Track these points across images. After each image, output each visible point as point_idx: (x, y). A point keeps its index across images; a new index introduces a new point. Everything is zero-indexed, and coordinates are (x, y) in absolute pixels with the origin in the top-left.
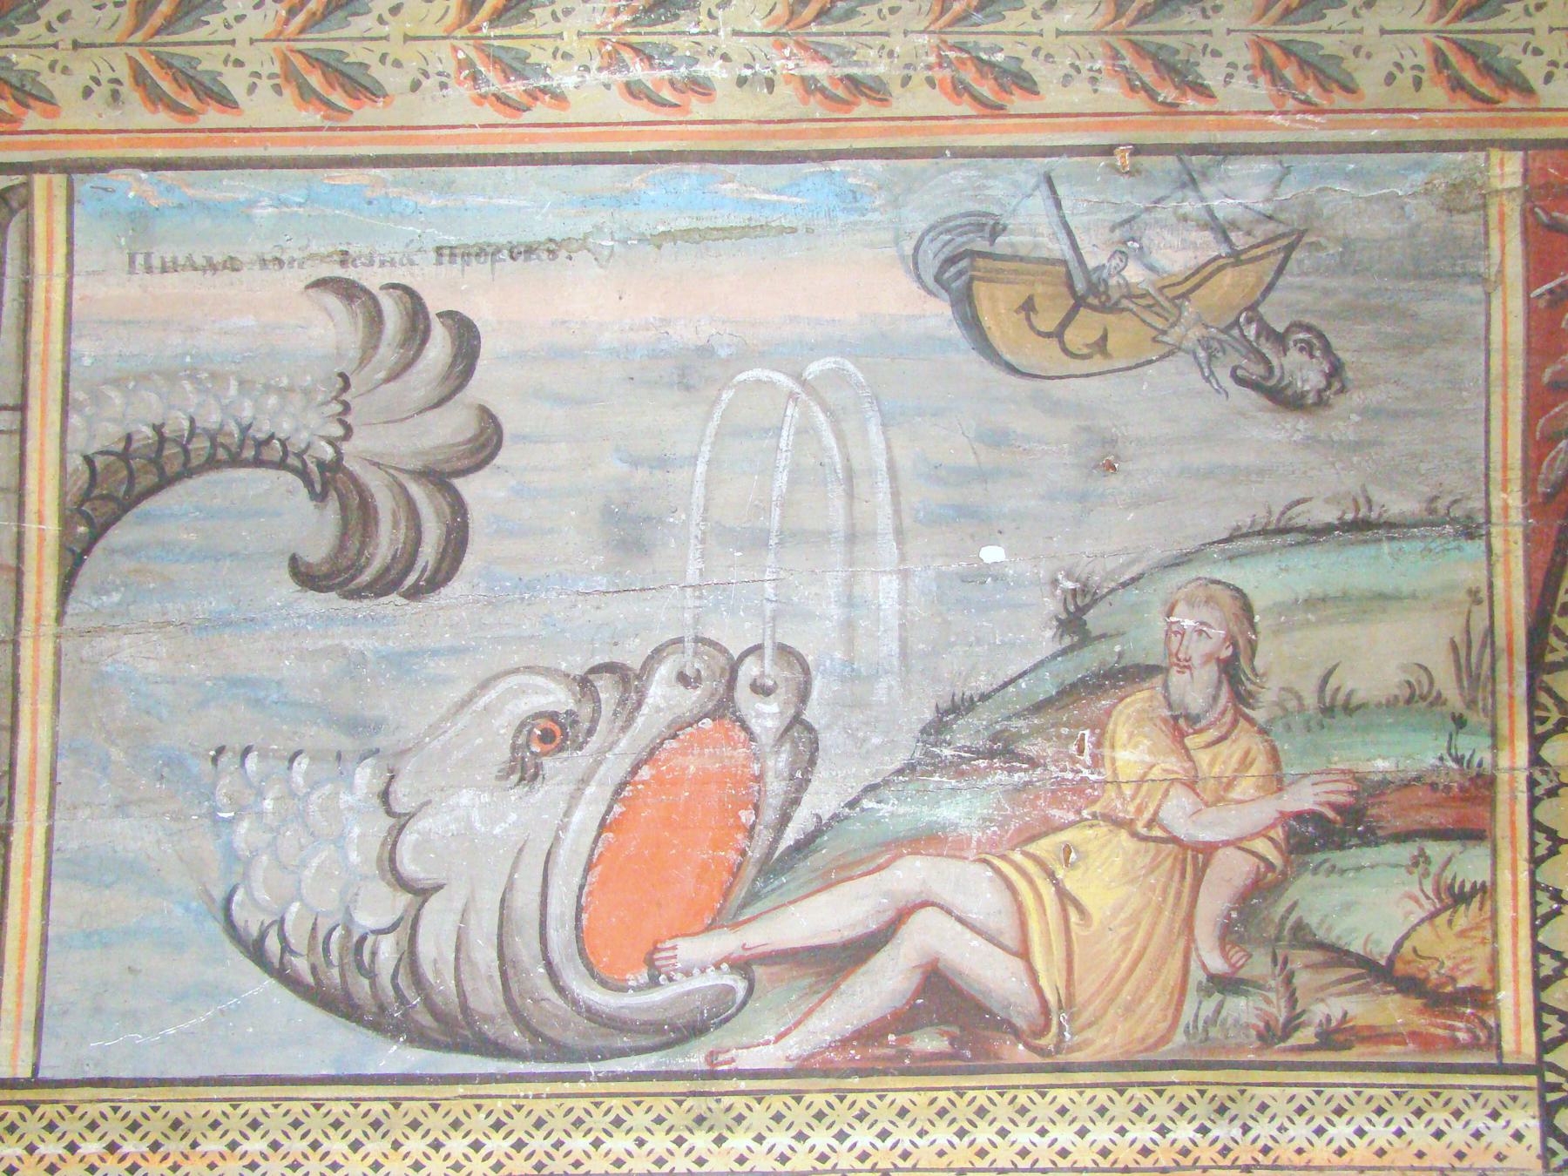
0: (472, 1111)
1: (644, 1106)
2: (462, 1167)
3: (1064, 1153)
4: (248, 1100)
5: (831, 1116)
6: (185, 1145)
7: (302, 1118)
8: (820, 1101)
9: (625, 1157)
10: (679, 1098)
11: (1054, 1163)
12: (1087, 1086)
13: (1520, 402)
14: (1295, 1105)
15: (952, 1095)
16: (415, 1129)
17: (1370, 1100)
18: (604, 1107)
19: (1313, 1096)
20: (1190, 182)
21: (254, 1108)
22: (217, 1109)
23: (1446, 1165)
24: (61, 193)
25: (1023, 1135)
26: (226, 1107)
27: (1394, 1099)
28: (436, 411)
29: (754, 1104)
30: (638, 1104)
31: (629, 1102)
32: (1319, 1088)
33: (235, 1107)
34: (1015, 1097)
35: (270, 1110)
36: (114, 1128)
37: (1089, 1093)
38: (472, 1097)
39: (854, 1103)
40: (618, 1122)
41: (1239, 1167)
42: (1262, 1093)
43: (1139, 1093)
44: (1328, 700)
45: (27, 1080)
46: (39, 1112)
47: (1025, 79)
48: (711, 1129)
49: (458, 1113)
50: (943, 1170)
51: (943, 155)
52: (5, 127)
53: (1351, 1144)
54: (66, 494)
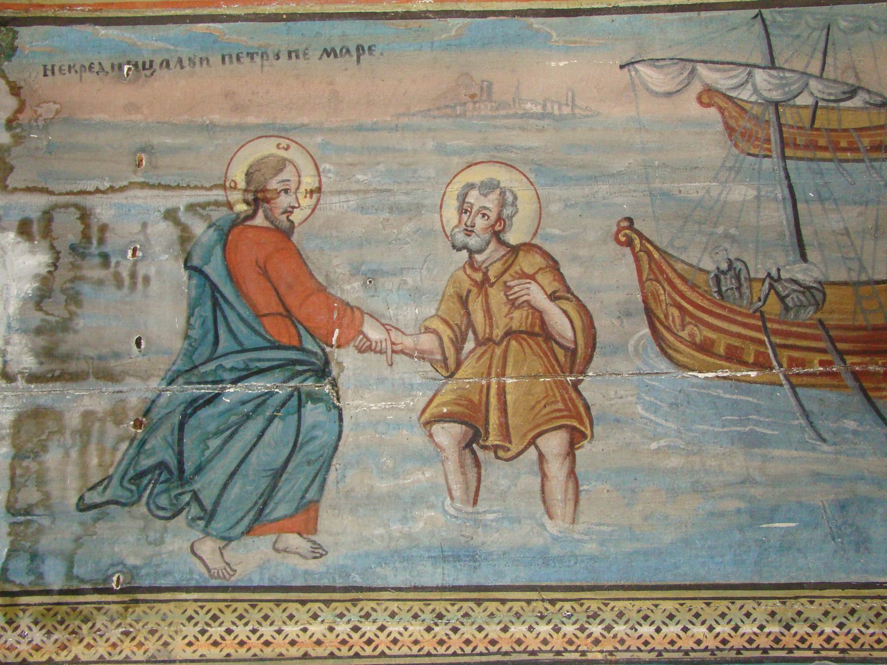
1: (231, 609)
2: (806, 640)
3: (493, 642)
5: (323, 616)
6: (718, 629)
9: (676, 639)
10: (708, 602)
11: (487, 649)
12: (738, 599)
14: (874, 612)
17: (235, 610)
18: (206, 609)
19: (423, 607)
20: (375, 123)
21: (440, 607)
23: (612, 649)
25: (699, 631)
29: (449, 607)
30: (228, 607)
31: (222, 605)
34: (461, 607)
35: (449, 607)
36: (382, 617)
37: (460, 604)
38: (653, 599)
40: (748, 615)
41: (527, 652)
42: (619, 605)
47: (747, 135)
49: (215, 611)
50: (221, 661)
52: (886, 138)
53: (653, 638)
54: (204, 208)
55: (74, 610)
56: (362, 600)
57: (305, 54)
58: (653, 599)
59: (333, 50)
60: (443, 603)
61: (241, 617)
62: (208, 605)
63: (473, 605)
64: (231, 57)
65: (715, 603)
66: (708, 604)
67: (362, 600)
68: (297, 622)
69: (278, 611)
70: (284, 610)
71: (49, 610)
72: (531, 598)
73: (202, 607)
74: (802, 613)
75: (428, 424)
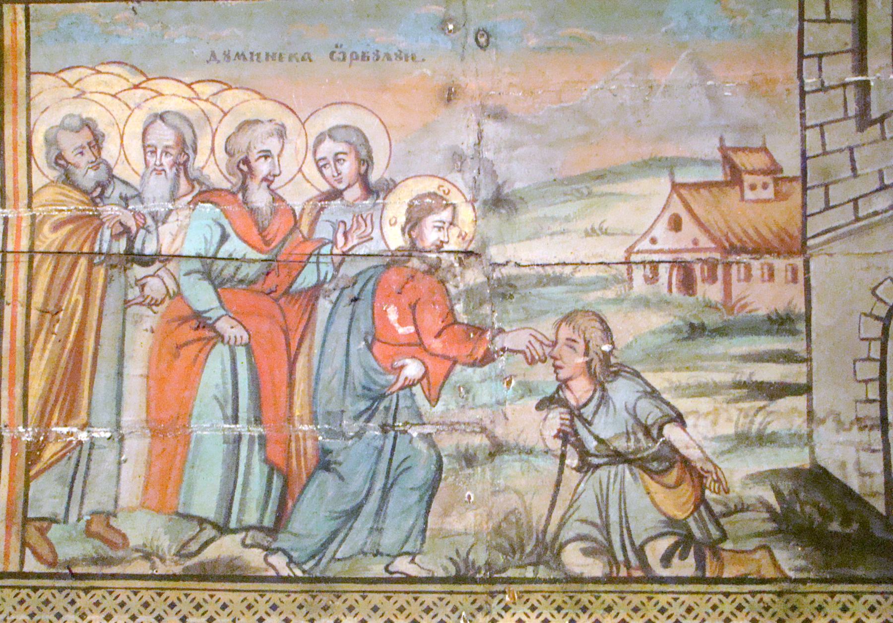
0: (412, 601)
1: (626, 601)
4: (395, 592)
7: (254, 603)
8: (872, 599)
13: (246, 382)
15: (357, 596)
16: (584, 612)
19: (593, 599)
21: (275, 598)
22: (251, 597)
24: (21, 17)
26: (256, 595)
27: (156, 597)
28: (799, 152)
30: (676, 599)
32: (262, 593)
33: (262, 596)
37: (293, 596)
39: (528, 600)
43: (844, 598)
44: (333, 466)
45: (625, 578)
46: (139, 595)
48: (853, 615)
51: (801, 109)
55: (212, 596)
56: (347, 592)
57: (413, 58)
58: (673, 592)
59: (243, 54)
60: (253, 594)
61: (533, 608)
62: (682, 597)
63: (256, 595)
64: (259, 55)
65: (395, 597)
66: (389, 598)
67: (347, 592)
68: (356, 615)
69: (754, 601)
70: (733, 601)
71: (676, 599)
72: (731, 590)
73: (441, 599)
74: (372, 609)
75: (857, 402)
